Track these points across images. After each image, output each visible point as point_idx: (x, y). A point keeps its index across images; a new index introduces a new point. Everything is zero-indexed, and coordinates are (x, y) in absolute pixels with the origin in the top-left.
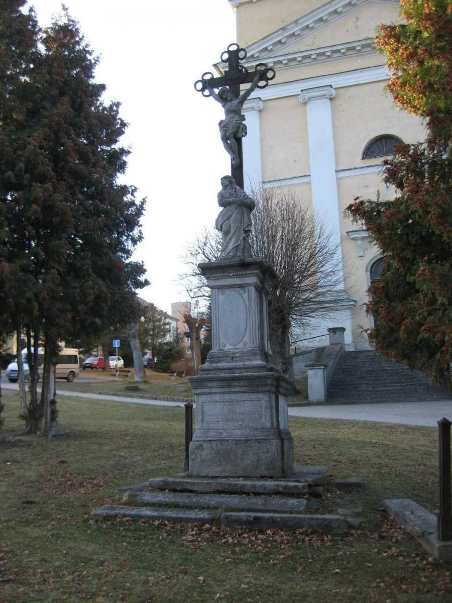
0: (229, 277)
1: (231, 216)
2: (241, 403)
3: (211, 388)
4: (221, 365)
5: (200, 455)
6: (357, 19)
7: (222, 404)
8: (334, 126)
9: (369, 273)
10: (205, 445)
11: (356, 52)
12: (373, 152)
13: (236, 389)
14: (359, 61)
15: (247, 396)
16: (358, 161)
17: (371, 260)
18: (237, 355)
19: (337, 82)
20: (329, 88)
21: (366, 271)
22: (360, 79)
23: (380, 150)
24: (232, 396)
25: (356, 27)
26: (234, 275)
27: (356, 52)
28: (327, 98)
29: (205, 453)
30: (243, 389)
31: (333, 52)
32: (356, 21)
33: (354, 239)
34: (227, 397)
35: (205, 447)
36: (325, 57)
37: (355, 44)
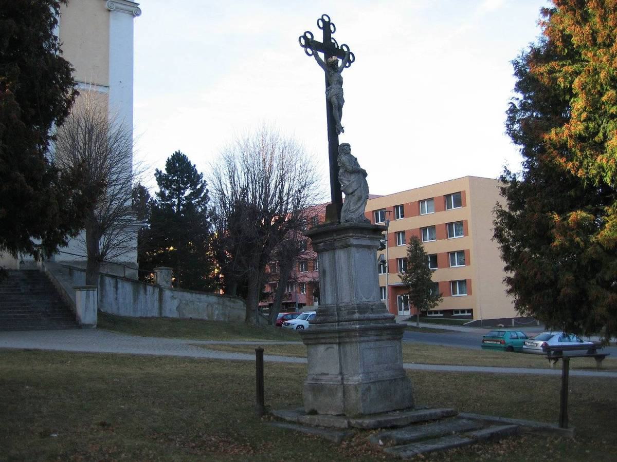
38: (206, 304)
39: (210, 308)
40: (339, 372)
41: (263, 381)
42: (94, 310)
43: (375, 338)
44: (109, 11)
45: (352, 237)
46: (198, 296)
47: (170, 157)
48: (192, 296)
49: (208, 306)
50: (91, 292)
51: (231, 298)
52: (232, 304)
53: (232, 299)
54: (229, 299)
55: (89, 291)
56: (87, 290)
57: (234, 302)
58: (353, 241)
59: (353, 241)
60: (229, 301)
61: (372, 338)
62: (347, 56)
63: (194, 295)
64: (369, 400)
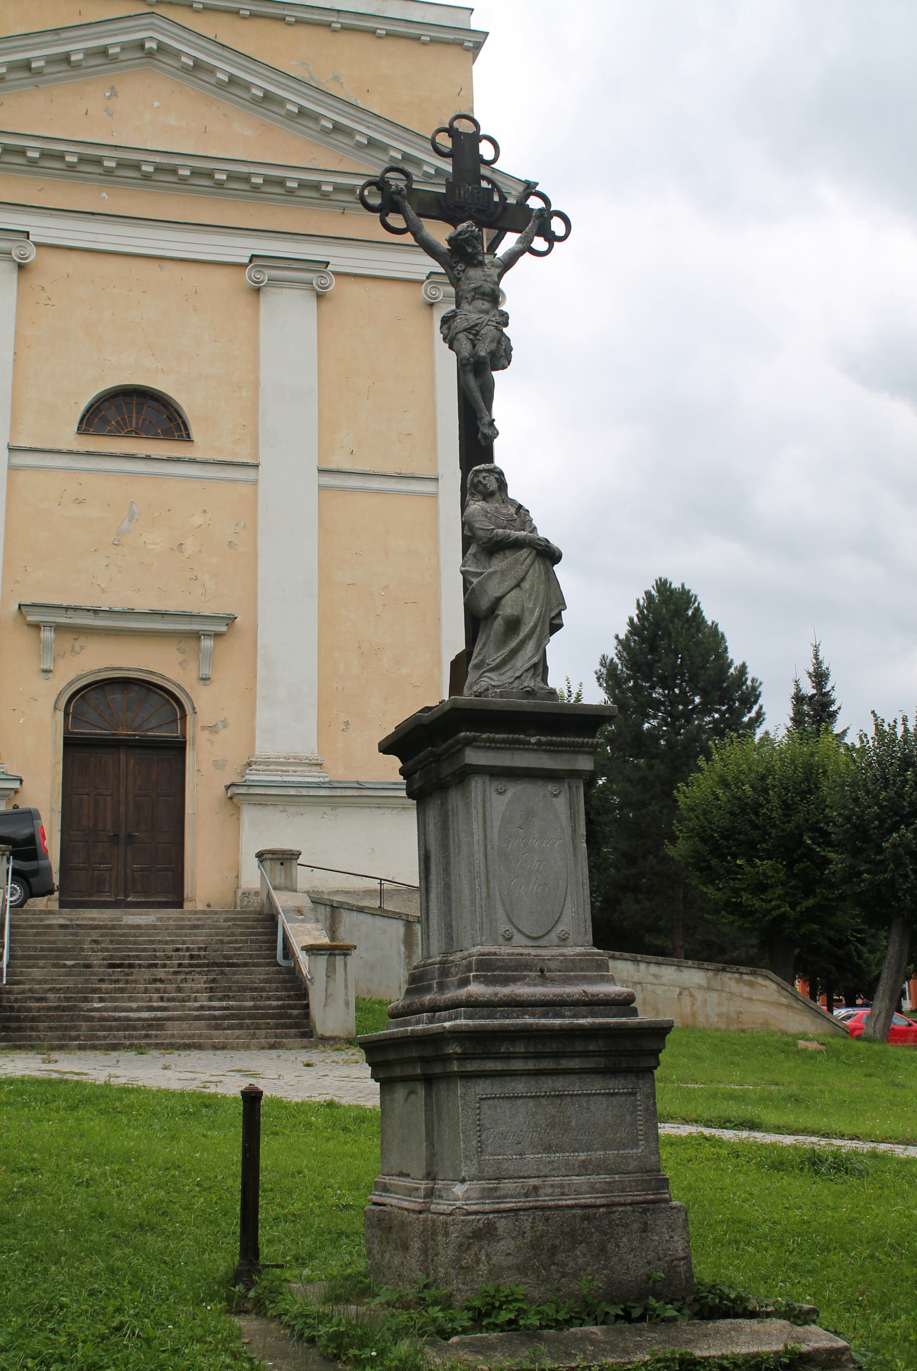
0: (524, 747)
1: (523, 579)
2: (583, 1100)
3: (509, 1057)
4: (522, 990)
5: (487, 1255)
6: (114, 94)
7: (531, 1103)
8: (18, 336)
9: (60, 715)
10: (502, 1224)
11: (283, 192)
12: (106, 421)
13: (575, 1063)
14: (104, 195)
15: (597, 1085)
16: (69, 437)
17: (71, 683)
18: (553, 965)
19: (43, 229)
20: (22, 237)
21: (55, 708)
22: (102, 238)
23: (123, 419)
24: (560, 1084)
25: (110, 112)
26: (539, 743)
27: (283, 192)
28: (313, 289)
29: (502, 1246)
30: (590, 1063)
31: (45, 155)
32: (109, 98)
33: (37, 626)
34: (548, 1085)
35: (500, 1230)
36: (247, 187)
37: (253, 170)
38: (678, 990)
39: (686, 1000)
40: (424, 1172)
41: (257, 1202)
42: (347, 1004)
43: (601, 1062)
44: (431, 305)
45: (469, 742)
46: (653, 969)
47: (611, 652)
48: (638, 971)
49: (680, 994)
50: (337, 958)
51: (741, 973)
52: (746, 990)
53: (746, 977)
54: (737, 975)
55: (335, 955)
56: (330, 955)
57: (751, 984)
58: (474, 757)
59: (474, 757)
60: (738, 981)
61: (518, 1065)
62: (534, 220)
63: (643, 966)
64: (483, 1268)
